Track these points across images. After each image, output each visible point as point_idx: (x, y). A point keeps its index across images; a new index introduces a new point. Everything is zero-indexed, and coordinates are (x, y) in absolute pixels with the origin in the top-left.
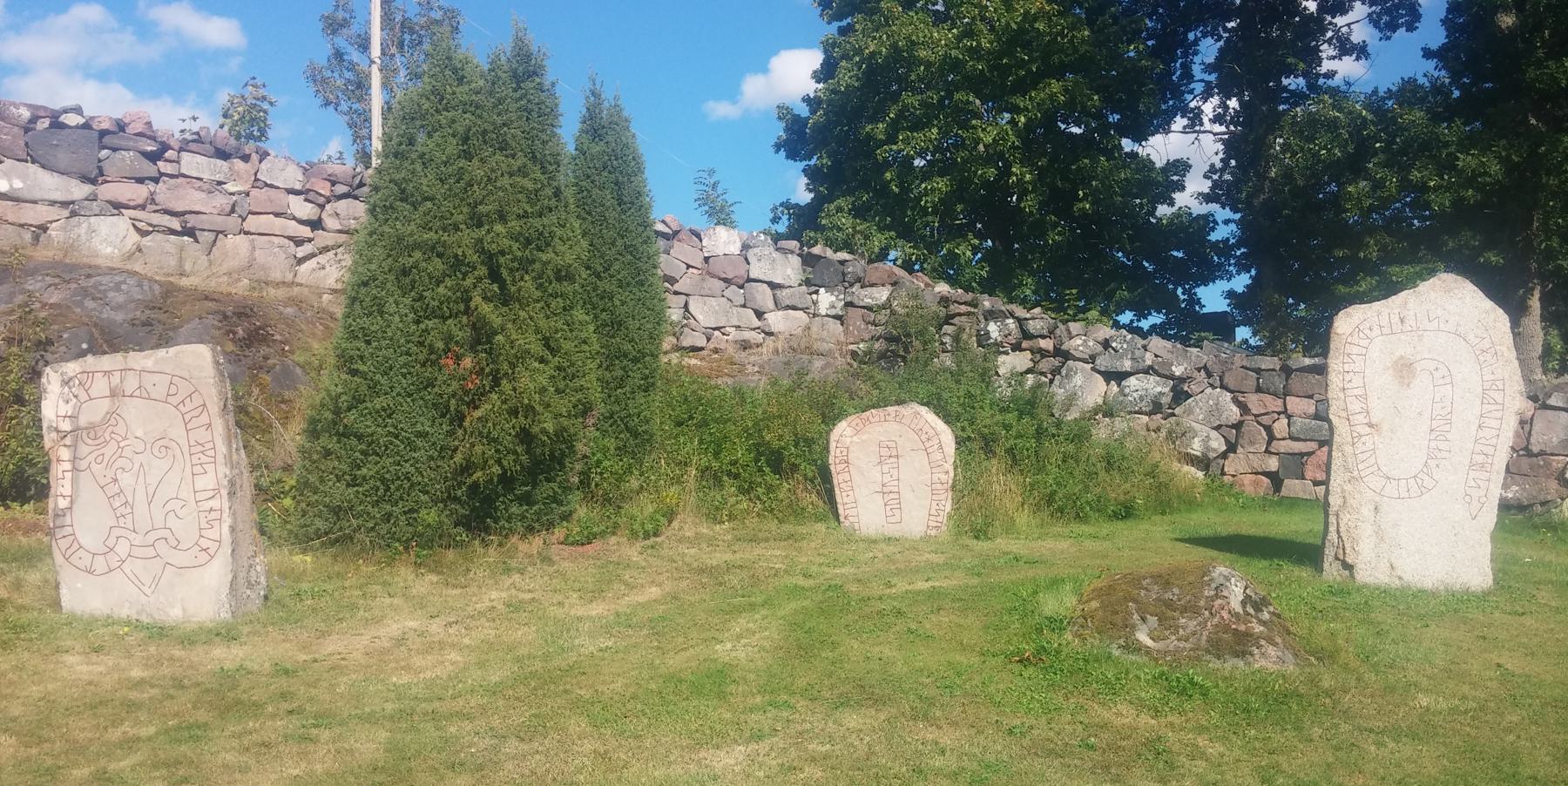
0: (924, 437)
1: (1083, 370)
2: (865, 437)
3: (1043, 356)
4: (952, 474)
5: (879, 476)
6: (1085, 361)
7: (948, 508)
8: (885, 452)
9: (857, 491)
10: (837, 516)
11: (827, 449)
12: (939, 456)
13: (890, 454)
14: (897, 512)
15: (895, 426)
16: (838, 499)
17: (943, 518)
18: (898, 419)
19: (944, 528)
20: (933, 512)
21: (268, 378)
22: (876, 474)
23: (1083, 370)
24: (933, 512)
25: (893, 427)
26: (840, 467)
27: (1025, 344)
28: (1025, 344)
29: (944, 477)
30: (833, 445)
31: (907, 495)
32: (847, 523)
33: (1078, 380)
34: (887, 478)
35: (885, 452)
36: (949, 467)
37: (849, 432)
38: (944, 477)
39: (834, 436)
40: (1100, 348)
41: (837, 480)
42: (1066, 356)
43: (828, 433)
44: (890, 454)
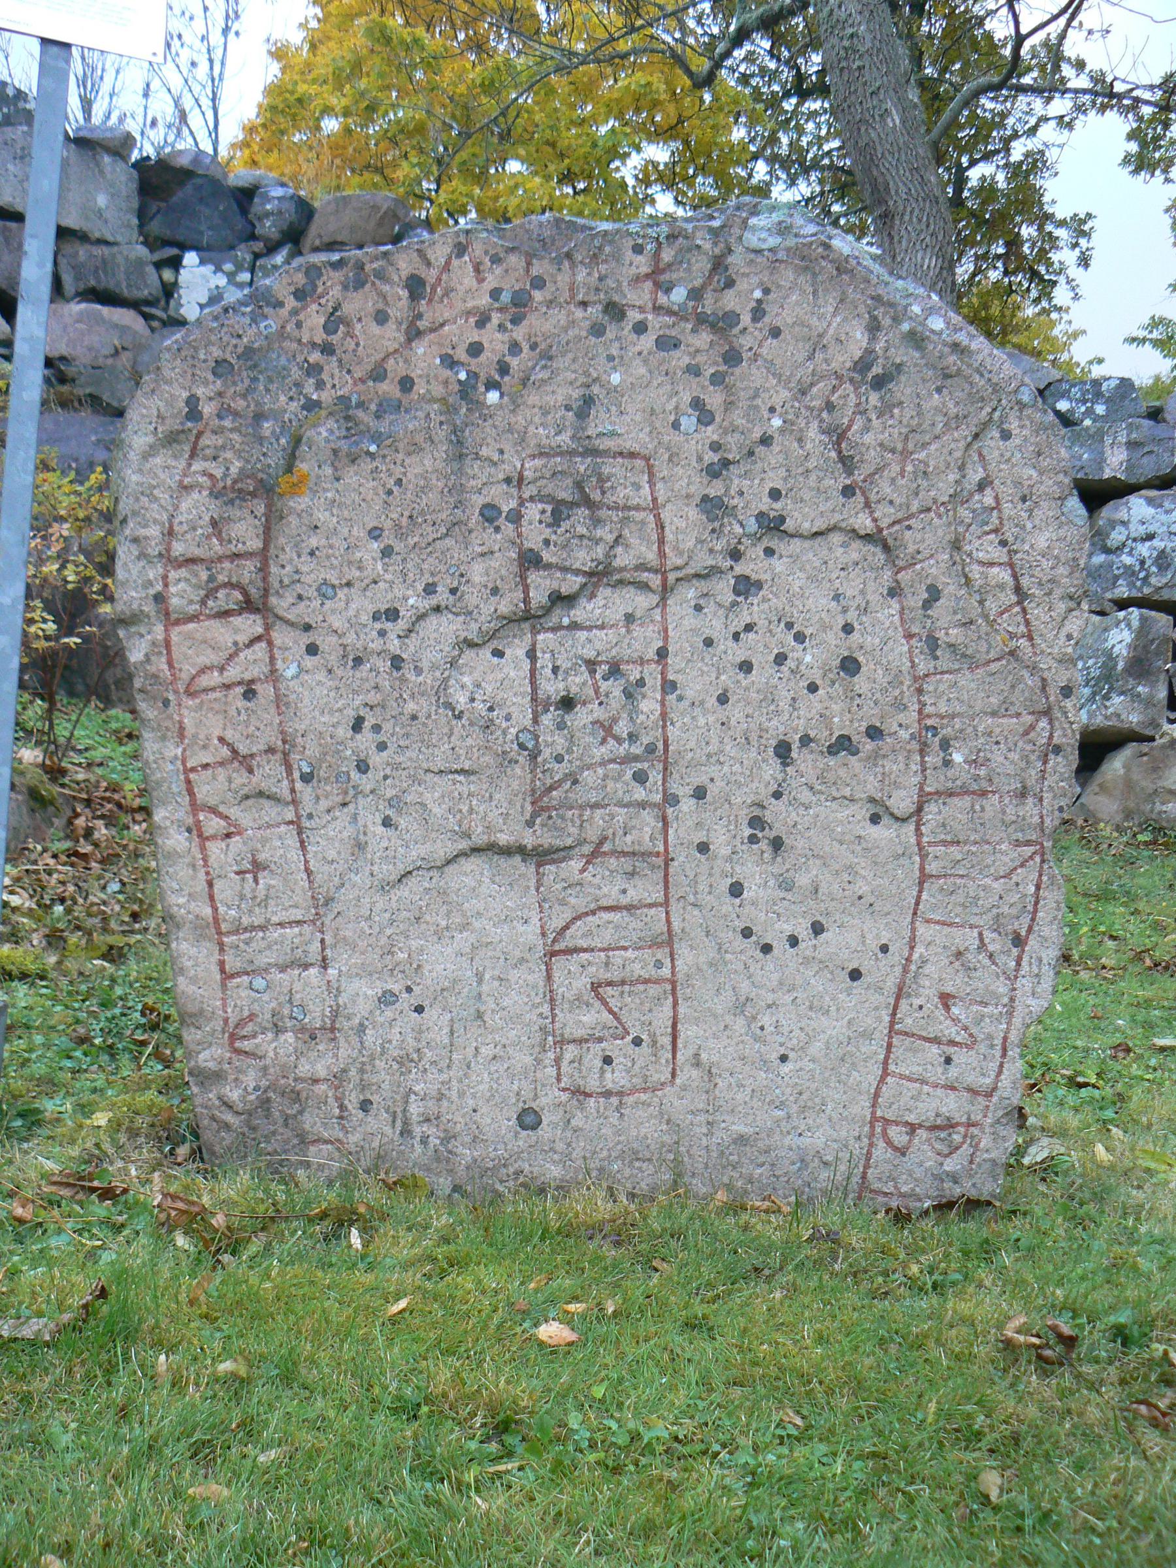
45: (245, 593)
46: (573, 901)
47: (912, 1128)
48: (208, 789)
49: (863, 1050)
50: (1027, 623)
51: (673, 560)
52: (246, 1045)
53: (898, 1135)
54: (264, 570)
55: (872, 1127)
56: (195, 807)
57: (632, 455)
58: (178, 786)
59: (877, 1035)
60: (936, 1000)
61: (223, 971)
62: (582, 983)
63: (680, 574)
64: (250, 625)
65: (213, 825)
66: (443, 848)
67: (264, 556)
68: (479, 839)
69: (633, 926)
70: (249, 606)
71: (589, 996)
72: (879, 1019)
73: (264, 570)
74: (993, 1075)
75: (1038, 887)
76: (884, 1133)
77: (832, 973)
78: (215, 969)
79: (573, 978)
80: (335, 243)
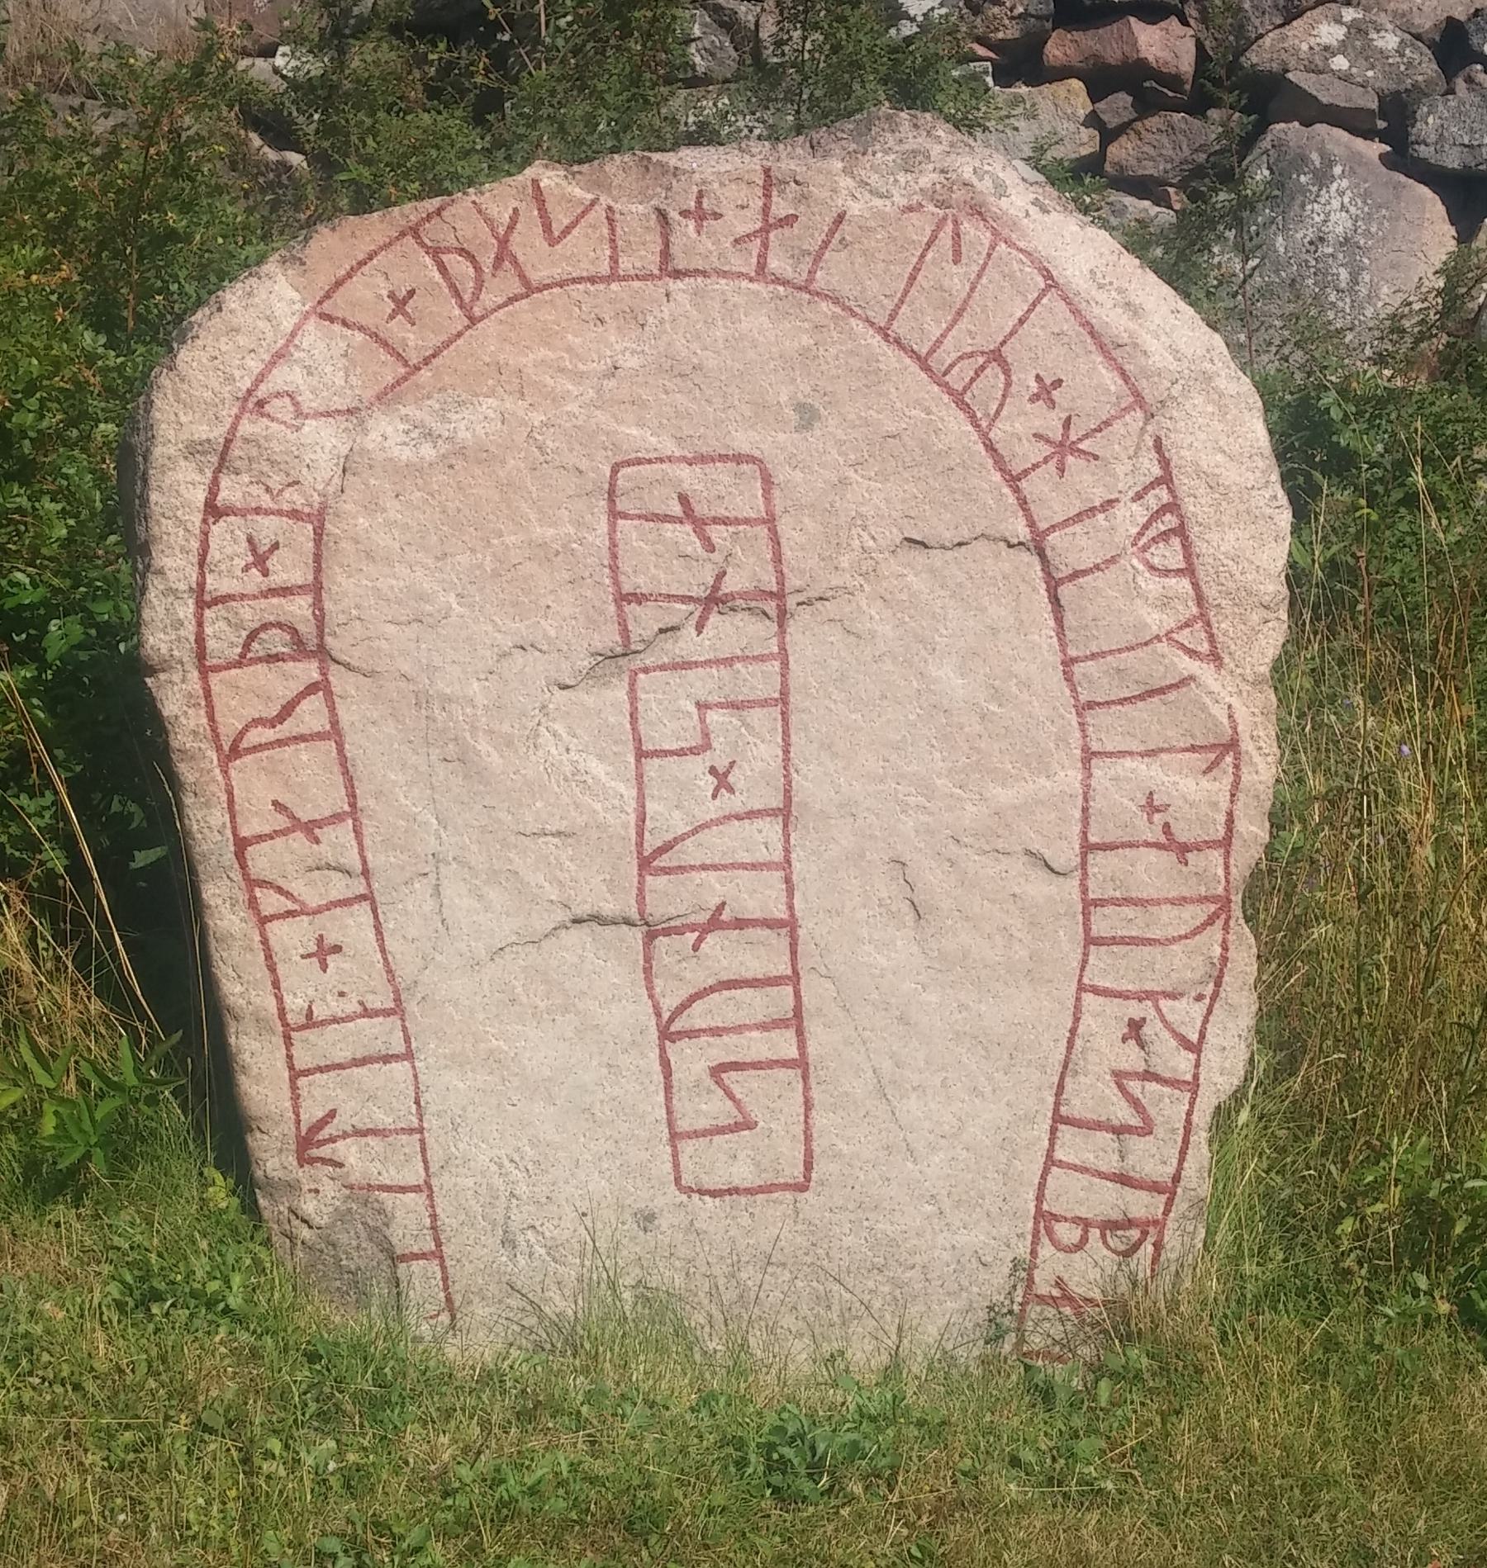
0: (1022, 427)
1: (1355, 163)
2: (474, 422)
3: (1146, 105)
4: (1263, 767)
5: (610, 776)
6: (1353, 122)
7: (1229, 1056)
8: (662, 560)
9: (408, 914)
10: (225, 1130)
11: (120, 516)
12: (1145, 601)
13: (708, 587)
14: (772, 1098)
15: (759, 324)
16: (240, 982)
17: (1177, 1150)
18: (792, 262)
19: (1182, 1238)
20: (1094, 1094)
21: (947, 675)
22: (577, 759)
23: (1355, 163)
24: (1094, 1094)
25: (735, 327)
26: (246, 695)
27: (1058, 48)
28: (1058, 48)
29: (1193, 792)
30: (176, 489)
31: (861, 946)
32: (320, 1199)
33: (1334, 210)
34: (680, 800)
35: (662, 560)
36: (1239, 696)
37: (324, 364)
38: (1193, 792)
39: (191, 398)
40: (1427, 67)
41: (229, 804)
42: (1270, 98)
43: (130, 395)
44: (708, 587)
45: (294, 631)
46: (688, 975)
47: (1086, 1224)
48: (261, 860)
49: (1024, 1135)
50: (1211, 638)
51: (793, 582)
52: (325, 1151)
53: (1068, 1233)
54: (318, 604)
55: (1036, 1222)
56: (252, 883)
57: (739, 459)
58: (229, 856)
59: (1039, 1118)
60: (1108, 1077)
61: (291, 1067)
62: (700, 1067)
63: (801, 598)
64: (310, 671)
65: (270, 902)
66: (542, 922)
67: (316, 589)
68: (582, 910)
69: (756, 1004)
70: (300, 649)
71: (709, 1082)
72: (1042, 1101)
73: (318, 604)
74: (1175, 1162)
75: (1225, 949)
76: (1050, 1232)
77: (986, 1049)
78: (281, 1064)
79: (692, 1060)
80: (1063, 471)
